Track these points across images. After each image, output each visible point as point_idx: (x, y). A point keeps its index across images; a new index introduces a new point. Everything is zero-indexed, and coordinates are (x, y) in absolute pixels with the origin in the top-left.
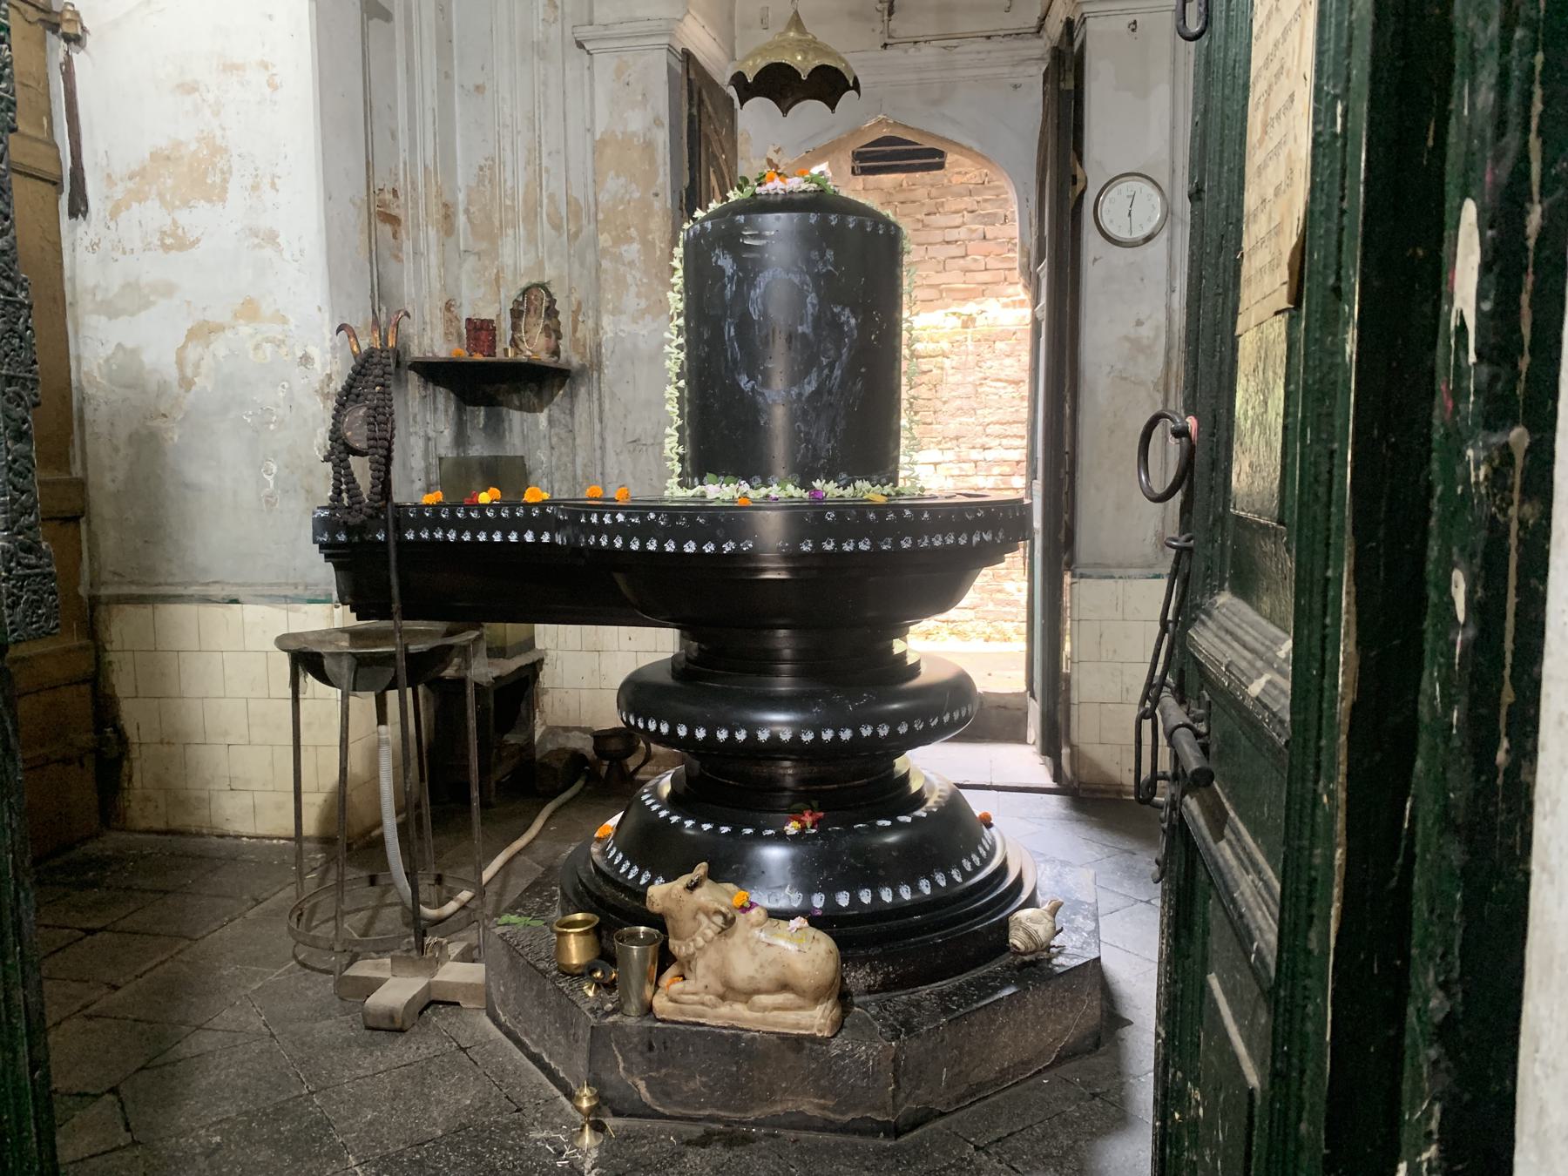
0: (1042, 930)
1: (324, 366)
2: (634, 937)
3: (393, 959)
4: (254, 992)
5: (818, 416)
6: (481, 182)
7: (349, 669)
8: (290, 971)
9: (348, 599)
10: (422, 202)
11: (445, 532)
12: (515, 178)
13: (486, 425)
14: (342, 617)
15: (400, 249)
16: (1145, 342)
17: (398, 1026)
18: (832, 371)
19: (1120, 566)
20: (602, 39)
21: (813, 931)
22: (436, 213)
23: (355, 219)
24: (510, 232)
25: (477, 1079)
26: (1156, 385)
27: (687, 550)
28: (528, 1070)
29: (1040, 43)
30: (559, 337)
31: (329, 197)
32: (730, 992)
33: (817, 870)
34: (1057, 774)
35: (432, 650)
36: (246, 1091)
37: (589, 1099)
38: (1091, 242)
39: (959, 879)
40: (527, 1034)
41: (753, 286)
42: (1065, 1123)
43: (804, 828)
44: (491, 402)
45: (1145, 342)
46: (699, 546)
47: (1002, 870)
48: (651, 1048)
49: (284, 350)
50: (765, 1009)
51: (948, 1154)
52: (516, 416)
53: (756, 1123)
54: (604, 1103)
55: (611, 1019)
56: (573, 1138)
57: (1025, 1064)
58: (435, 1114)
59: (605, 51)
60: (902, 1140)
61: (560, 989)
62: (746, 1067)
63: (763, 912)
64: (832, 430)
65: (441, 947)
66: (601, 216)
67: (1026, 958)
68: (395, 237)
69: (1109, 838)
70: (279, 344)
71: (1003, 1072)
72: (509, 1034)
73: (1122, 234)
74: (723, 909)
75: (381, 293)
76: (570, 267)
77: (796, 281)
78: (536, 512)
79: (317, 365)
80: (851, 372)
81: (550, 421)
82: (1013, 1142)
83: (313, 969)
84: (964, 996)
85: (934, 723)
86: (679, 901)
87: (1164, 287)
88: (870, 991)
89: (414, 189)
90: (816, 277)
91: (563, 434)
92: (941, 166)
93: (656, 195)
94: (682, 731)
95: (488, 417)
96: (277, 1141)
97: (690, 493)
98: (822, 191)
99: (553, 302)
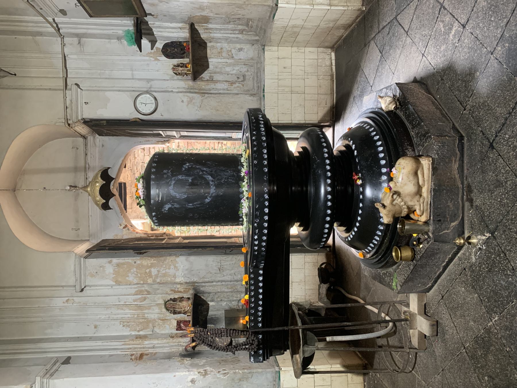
0: (389, 100)
1: (195, 375)
2: (402, 229)
5: (220, 175)
6: (128, 326)
7: (308, 347)
8: (416, 372)
9: (282, 352)
10: (135, 346)
11: (259, 311)
12: (128, 313)
13: (214, 324)
15: (152, 353)
16: (189, 100)
17: (435, 323)
18: (204, 171)
20: (81, 282)
25: (454, 288)
26: (202, 96)
28: (449, 271)
29: (89, 138)
30: (183, 297)
32: (419, 192)
33: (374, 176)
34: (329, 126)
35: (300, 318)
37: (460, 240)
38: (156, 117)
39: (373, 129)
40: (436, 273)
41: (175, 197)
42: (453, 85)
43: (359, 178)
45: (189, 100)
46: (266, 207)
47: (369, 118)
48: (440, 221)
50: (424, 181)
51: (468, 119)
52: (210, 313)
53: (462, 183)
54: (461, 234)
55: (431, 235)
56: (475, 245)
57: (433, 103)
58: (469, 299)
59: (85, 282)
60: (464, 135)
61: (421, 257)
62: (444, 187)
64: (224, 171)
65: (405, 312)
66: (142, 282)
67: (398, 104)
69: (349, 105)
71: (437, 108)
72: (435, 282)
73: (154, 106)
74: (391, 194)
75: (169, 357)
76: (159, 294)
77: (173, 182)
78: (252, 276)
79: (195, 377)
80: (204, 165)
81: (212, 301)
82: (462, 99)
84: (413, 120)
85: (322, 136)
86: (389, 211)
87: (171, 94)
88: (414, 150)
89: (130, 349)
90: (173, 175)
91: (216, 296)
92: (125, 184)
93: (135, 262)
94: (328, 219)
95: (211, 323)
96: (485, 355)
97: (245, 220)
98: (142, 177)
99: (171, 299)
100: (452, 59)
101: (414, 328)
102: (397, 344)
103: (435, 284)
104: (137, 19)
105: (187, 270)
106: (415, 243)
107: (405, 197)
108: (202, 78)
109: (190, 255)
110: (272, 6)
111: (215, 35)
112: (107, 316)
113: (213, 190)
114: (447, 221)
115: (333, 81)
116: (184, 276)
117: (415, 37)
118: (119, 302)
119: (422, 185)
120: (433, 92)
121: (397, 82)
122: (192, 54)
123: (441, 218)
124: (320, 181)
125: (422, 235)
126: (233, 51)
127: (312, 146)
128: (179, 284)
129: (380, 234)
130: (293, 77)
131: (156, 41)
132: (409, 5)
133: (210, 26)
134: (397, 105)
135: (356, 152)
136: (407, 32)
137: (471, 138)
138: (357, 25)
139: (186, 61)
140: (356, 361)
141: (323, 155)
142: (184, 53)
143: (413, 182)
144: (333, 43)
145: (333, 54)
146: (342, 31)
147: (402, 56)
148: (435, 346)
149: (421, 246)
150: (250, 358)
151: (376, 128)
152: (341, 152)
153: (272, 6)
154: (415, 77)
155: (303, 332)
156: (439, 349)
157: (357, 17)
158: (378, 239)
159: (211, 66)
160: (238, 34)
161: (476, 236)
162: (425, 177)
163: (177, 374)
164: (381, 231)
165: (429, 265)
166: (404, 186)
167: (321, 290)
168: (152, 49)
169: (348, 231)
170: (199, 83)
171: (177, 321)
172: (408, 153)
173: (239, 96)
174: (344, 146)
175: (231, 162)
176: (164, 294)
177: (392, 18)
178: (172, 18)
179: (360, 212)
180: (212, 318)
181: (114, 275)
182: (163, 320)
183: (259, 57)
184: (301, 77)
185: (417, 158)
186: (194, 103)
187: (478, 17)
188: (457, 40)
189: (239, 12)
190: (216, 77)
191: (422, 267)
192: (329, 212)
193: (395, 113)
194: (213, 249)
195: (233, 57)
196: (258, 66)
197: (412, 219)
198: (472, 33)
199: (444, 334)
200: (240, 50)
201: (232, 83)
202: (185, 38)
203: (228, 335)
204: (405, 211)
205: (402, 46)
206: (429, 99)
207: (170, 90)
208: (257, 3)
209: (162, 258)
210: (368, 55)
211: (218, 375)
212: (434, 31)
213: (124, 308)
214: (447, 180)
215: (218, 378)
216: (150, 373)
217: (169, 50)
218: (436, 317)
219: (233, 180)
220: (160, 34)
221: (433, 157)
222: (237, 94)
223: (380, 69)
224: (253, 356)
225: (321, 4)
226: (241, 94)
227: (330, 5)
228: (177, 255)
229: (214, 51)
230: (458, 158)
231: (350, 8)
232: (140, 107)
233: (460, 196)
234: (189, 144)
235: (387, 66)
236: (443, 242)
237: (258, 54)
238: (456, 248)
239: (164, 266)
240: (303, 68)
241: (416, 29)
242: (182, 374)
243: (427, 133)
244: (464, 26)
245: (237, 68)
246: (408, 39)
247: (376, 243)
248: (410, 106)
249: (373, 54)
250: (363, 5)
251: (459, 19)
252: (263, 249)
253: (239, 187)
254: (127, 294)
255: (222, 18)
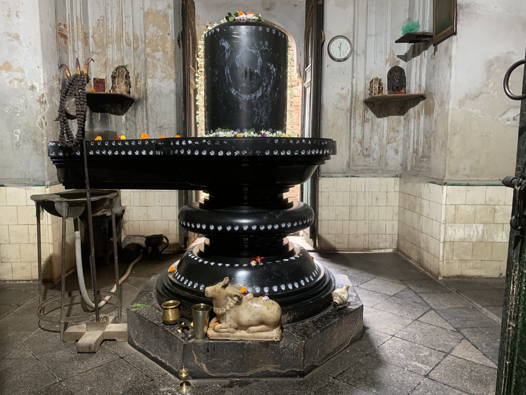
0: (345, 296)
1: (40, 90)
2: (199, 308)
3: (87, 324)
4: (25, 342)
5: (262, 106)
6: (98, 26)
8: (39, 332)
9: (62, 180)
10: (75, 31)
11: (107, 151)
12: (113, 25)
13: (101, 120)
14: (61, 188)
15: (68, 49)
16: (344, 95)
17: (93, 350)
18: (267, 88)
19: (335, 173)
21: (271, 301)
22: (81, 36)
23: (51, 32)
24: (111, 46)
25: (131, 369)
26: (348, 110)
27: (220, 155)
30: (130, 87)
31: (42, 22)
32: (240, 326)
34: (315, 246)
35: (100, 200)
36: (31, 383)
37: (185, 373)
38: (326, 59)
39: (313, 280)
40: (149, 349)
42: (361, 365)
43: (257, 263)
44: (103, 111)
47: (325, 275)
48: (208, 351)
49: (23, 83)
50: (254, 332)
52: (113, 117)
53: (251, 376)
54: (192, 375)
57: (341, 345)
58: (117, 385)
60: (305, 377)
61: (167, 331)
63: (252, 295)
64: (267, 112)
65: (107, 318)
66: (147, 41)
67: (340, 307)
68: (65, 43)
70: (21, 81)
71: (335, 350)
72: (140, 350)
73: (338, 57)
74: (238, 294)
77: (254, 52)
79: (38, 90)
80: (274, 89)
82: (345, 375)
83: (49, 331)
84: (321, 322)
86: (219, 292)
87: (351, 76)
88: (288, 322)
89: (73, 25)
90: (262, 52)
91: (132, 124)
93: (169, 34)
94: (212, 228)
95: (101, 116)
99: (128, 73)
100: (390, 364)
101: (88, 328)
102: (73, 312)
103: (138, 350)
104: (431, 36)
105: (160, 91)
106: (183, 324)
107: (236, 311)
108: (367, 110)
109: (177, 95)
110: (444, 180)
111: (412, 124)
112: (109, 3)
113: (245, 97)
114: (208, 359)
115: (363, 251)
116: (153, 88)
117: (413, 328)
118: (126, 17)
119: (249, 330)
120: (353, 345)
121: (364, 307)
122: (392, 99)
123: (210, 352)
124: (254, 218)
125: (192, 332)
126: (395, 144)
127: (293, 212)
128: (145, 82)
129: (195, 287)
130: (367, 208)
131: (406, 61)
132: (447, 321)
133: (422, 117)
134: (339, 305)
135: (287, 260)
136: (417, 320)
137: (302, 385)
138: (422, 272)
139: (385, 92)
140: (57, 271)
141: (284, 222)
142: (393, 89)
143: (252, 319)
144: (402, 250)
145: (390, 251)
146: (416, 258)
147: (391, 315)
148: (67, 351)
149: (180, 331)
150: (53, 142)
151: (313, 283)
152: (287, 246)
153: (444, 180)
154: (368, 328)
155: (83, 202)
156: (62, 354)
157: (431, 272)
158: (189, 285)
159: (379, 120)
160: (414, 148)
161: (190, 392)
162: (258, 333)
163: (42, 70)
164: (198, 287)
165: (158, 341)
166: (247, 308)
167: (139, 237)
168: (398, 56)
169: (200, 254)
170: (362, 107)
171: (104, 80)
172: (286, 316)
173: (348, 150)
174: (293, 249)
175: (278, 120)
176: (134, 66)
177: (431, 305)
178: (430, 75)
179: (220, 265)
180: (108, 118)
181: (154, 11)
182: (105, 64)
183: (388, 171)
184: (367, 216)
185: (278, 324)
186: (341, 101)
187: (437, 390)
188: (411, 369)
189: (438, 145)
190: (368, 126)
191: (156, 334)
192: (220, 228)
193: (330, 304)
194: (183, 119)
195: (388, 143)
196: (379, 170)
197: (210, 320)
198: (419, 384)
199: (79, 360)
200: (396, 152)
201: (361, 143)
202: (409, 91)
203: (78, 112)
204: (219, 311)
205: (402, 315)
206: (346, 342)
207: (355, 76)
208: (447, 163)
209: (173, 65)
210: (391, 283)
211: (40, 117)
212: (420, 346)
213: (118, 22)
214: (254, 359)
215: (37, 116)
216: (42, 39)
217: (397, 74)
218: (99, 351)
219: (257, 121)
220: (414, 64)
221: (281, 342)
222: (350, 148)
223: (376, 294)
224: (56, 145)
225: (446, 233)
226: (350, 152)
227: (444, 242)
228: (176, 80)
229: (395, 124)
230: (279, 371)
231: (441, 263)
232: (336, 42)
233: (236, 374)
234: (297, 107)
235: (380, 301)
236: (184, 355)
237: (391, 171)
238: (177, 370)
239: (164, 66)
240: (376, 218)
241: (421, 329)
242: (41, 76)
243: (308, 336)
244: (426, 376)
245: (377, 148)
246: (410, 321)
247: (185, 283)
248: (339, 319)
249: (392, 288)
250: (444, 277)
251: (434, 371)
252: (176, 152)
253: (249, 129)
254: (135, 25)
255: (431, 128)
